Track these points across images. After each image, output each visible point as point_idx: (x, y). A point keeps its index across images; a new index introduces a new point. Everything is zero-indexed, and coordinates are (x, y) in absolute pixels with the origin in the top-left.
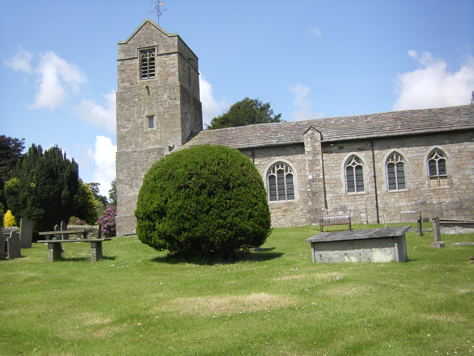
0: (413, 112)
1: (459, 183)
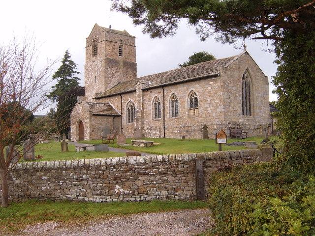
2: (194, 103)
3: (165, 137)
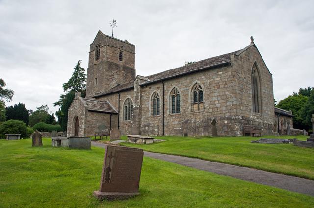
0: (212, 58)
1: (208, 107)
2: (198, 97)
3: (163, 134)
